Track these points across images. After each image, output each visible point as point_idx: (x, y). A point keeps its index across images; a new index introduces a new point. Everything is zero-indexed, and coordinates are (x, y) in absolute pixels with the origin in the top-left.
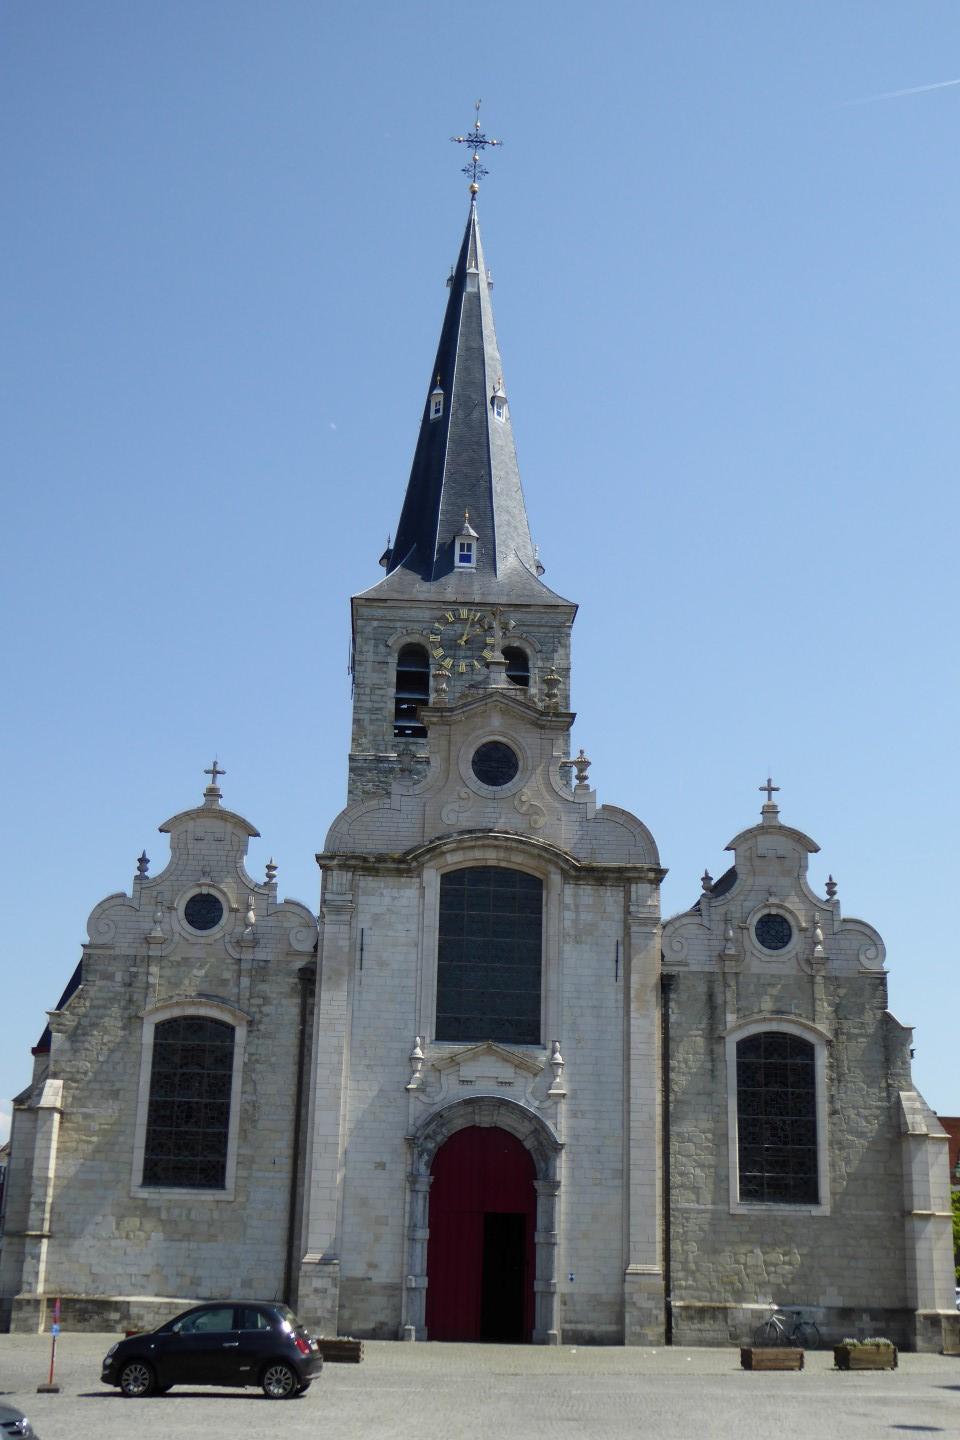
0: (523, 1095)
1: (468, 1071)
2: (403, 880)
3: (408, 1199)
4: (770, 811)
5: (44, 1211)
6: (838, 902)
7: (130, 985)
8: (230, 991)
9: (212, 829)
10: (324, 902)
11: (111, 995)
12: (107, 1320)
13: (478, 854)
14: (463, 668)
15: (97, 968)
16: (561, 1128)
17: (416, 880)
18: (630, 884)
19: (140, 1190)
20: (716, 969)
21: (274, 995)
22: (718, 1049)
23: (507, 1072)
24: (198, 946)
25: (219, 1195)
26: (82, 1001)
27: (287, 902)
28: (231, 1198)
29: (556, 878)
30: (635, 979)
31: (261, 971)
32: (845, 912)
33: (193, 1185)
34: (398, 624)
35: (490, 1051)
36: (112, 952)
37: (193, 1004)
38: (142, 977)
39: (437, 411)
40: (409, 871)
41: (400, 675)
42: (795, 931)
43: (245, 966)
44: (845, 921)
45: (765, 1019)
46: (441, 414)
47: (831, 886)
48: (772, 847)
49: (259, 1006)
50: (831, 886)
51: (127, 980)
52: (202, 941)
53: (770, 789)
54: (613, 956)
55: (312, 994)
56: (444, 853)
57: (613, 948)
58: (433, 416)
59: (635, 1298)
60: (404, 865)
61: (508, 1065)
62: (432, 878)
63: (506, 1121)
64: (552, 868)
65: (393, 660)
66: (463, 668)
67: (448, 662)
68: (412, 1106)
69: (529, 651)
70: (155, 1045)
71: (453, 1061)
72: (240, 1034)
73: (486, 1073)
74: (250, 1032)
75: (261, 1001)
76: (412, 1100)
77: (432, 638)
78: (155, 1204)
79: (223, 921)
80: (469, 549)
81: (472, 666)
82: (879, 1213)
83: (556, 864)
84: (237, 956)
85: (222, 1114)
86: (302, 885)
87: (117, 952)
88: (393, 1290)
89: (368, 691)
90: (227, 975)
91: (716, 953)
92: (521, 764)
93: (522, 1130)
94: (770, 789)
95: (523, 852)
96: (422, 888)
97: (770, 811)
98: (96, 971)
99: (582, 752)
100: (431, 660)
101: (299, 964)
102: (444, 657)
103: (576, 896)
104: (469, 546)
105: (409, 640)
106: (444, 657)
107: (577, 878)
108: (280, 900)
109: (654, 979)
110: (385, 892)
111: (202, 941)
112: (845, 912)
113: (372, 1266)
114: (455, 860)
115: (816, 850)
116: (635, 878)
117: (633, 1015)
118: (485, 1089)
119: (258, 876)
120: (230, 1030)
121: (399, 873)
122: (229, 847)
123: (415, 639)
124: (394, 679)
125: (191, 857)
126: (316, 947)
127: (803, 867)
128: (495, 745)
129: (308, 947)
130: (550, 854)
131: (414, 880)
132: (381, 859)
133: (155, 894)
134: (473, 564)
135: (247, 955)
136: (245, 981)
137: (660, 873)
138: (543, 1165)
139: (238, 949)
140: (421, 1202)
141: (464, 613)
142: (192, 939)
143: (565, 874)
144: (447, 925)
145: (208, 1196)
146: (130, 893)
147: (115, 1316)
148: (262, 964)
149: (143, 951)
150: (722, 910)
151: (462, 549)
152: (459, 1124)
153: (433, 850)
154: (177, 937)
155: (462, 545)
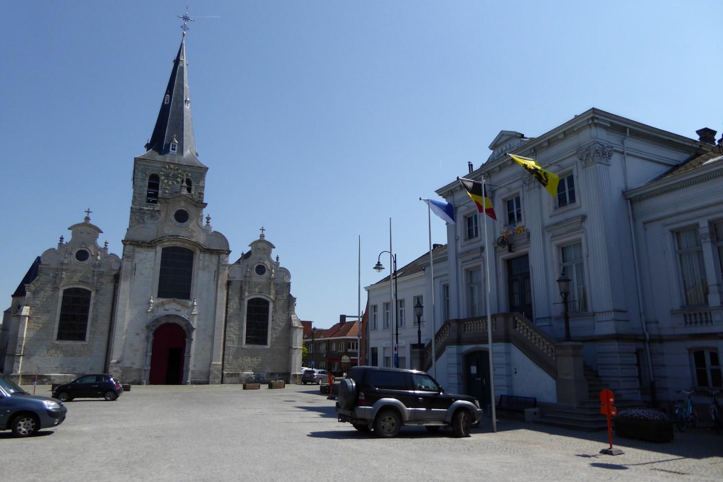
0: (184, 314)
1: (167, 307)
4: (262, 236)
9: (86, 231)
10: (123, 254)
13: (174, 243)
14: (170, 183)
16: (194, 324)
23: (179, 307)
25: (84, 343)
27: (111, 254)
29: (198, 251)
31: (101, 275)
32: (281, 265)
34: (150, 168)
39: (167, 102)
43: (95, 273)
44: (281, 268)
47: (277, 258)
48: (262, 246)
49: (100, 285)
50: (277, 258)
53: (263, 230)
54: (214, 275)
56: (163, 242)
58: (165, 103)
62: (159, 249)
63: (178, 321)
64: (197, 248)
66: (170, 183)
67: (166, 181)
70: (63, 296)
71: (163, 304)
72: (93, 294)
73: (172, 307)
77: (161, 173)
79: (89, 259)
84: (93, 270)
85: (85, 319)
86: (117, 249)
89: (138, 187)
90: (89, 276)
93: (182, 324)
94: (263, 230)
96: (156, 252)
97: (262, 236)
101: (114, 273)
102: (165, 179)
103: (204, 257)
104: (175, 146)
105: (153, 173)
106: (165, 179)
112: (281, 265)
114: (167, 244)
119: (274, 260)
120: (90, 293)
121: (149, 247)
124: (147, 184)
126: (120, 268)
127: (270, 252)
128: (182, 211)
130: (197, 244)
135: (96, 270)
136: (95, 278)
137: (229, 252)
140: (150, 345)
141: (172, 166)
143: (201, 251)
144: (163, 263)
145: (79, 343)
146: (56, 248)
151: (172, 146)
153: (160, 241)
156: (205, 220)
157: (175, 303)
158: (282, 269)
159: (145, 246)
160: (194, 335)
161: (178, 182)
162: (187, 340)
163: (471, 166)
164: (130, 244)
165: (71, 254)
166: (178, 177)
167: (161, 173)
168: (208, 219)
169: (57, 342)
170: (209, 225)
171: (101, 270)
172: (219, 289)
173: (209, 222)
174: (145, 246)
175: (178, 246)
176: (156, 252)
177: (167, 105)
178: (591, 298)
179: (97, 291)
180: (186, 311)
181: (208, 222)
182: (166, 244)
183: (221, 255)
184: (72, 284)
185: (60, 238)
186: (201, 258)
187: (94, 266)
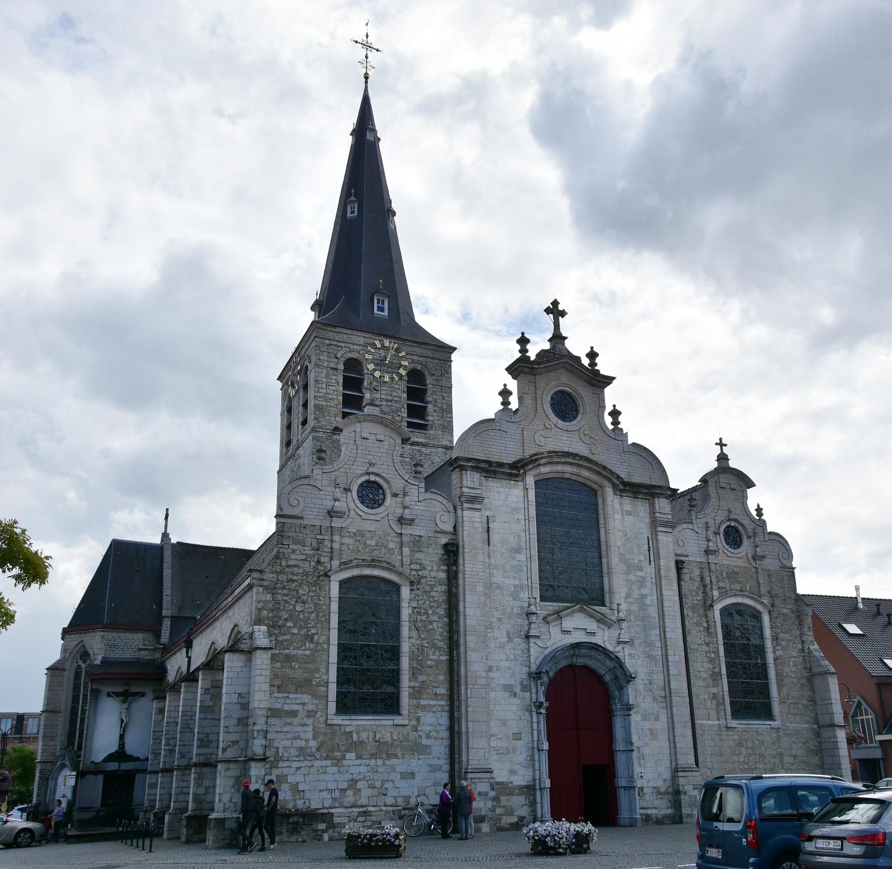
0: (604, 638)
1: (569, 623)
2: (512, 482)
3: (535, 720)
4: (722, 458)
5: (180, 752)
6: (764, 521)
7: (318, 549)
8: (395, 559)
11: (303, 557)
12: (317, 830)
13: (560, 468)
14: (387, 379)
15: (290, 534)
17: (520, 483)
18: (654, 498)
19: (335, 717)
20: (704, 560)
21: (427, 563)
22: (710, 614)
23: (592, 625)
24: (369, 522)
25: (398, 720)
26: (279, 561)
28: (406, 722)
29: (609, 491)
30: (662, 562)
31: (417, 543)
33: (375, 712)
35: (581, 610)
36: (301, 522)
37: (369, 566)
38: (327, 543)
39: (352, 212)
40: (517, 475)
41: (345, 378)
42: (744, 537)
43: (405, 539)
44: (771, 533)
45: (735, 595)
46: (356, 213)
47: (759, 510)
49: (417, 571)
51: (315, 544)
52: (372, 517)
54: (646, 547)
55: (456, 563)
56: (539, 465)
57: (646, 542)
58: (349, 215)
59: (686, 788)
60: (514, 471)
61: (592, 620)
62: (530, 480)
64: (606, 483)
65: (341, 367)
66: (387, 379)
68: (532, 649)
69: (426, 374)
72: (405, 592)
73: (578, 627)
74: (412, 590)
75: (418, 567)
76: (532, 644)
77: (367, 356)
78: (348, 729)
80: (383, 304)
81: (392, 379)
82: (807, 726)
83: (609, 480)
84: (399, 532)
87: (305, 522)
88: (530, 790)
90: (392, 545)
91: (702, 550)
92: (581, 409)
94: (721, 444)
95: (590, 469)
96: (526, 489)
97: (722, 458)
98: (289, 537)
99: (614, 406)
100: (365, 371)
101: (444, 540)
102: (375, 370)
103: (621, 504)
105: (350, 355)
106: (375, 370)
107: (622, 491)
108: (630, 443)
109: (673, 565)
110: (501, 490)
111: (372, 517)
113: (513, 772)
115: (750, 484)
116: (657, 493)
117: (663, 587)
118: (578, 637)
120: (397, 587)
121: (511, 477)
122: (387, 447)
123: (355, 355)
125: (359, 451)
126: (455, 527)
127: (745, 497)
129: (450, 528)
131: (519, 483)
132: (500, 465)
133: (333, 477)
134: (386, 313)
135: (407, 530)
136: (406, 551)
138: (617, 693)
139: (400, 526)
142: (364, 516)
145: (387, 721)
147: (322, 826)
148: (417, 538)
149: (326, 523)
150: (704, 520)
151: (378, 303)
152: (564, 663)
153: (533, 461)
154: (352, 512)
155: (378, 300)
156: (608, 420)
157: (582, 615)
158: (773, 537)
159: (503, 473)
160: (635, 693)
161: (401, 376)
162: (617, 706)
163: (523, 341)
164: (474, 468)
165: (347, 490)
166: (401, 365)
167: (367, 356)
168: (615, 414)
169: (338, 720)
170: (621, 430)
171: (416, 530)
172: (663, 582)
173: (619, 423)
174: (503, 473)
175: (567, 476)
176: (526, 489)
177: (352, 220)
178: (466, 677)
179: (412, 583)
180: (613, 633)
181: (616, 423)
182: (543, 470)
183: (656, 500)
184: (357, 566)
185: (501, 394)
186: (617, 506)
187: (401, 520)
